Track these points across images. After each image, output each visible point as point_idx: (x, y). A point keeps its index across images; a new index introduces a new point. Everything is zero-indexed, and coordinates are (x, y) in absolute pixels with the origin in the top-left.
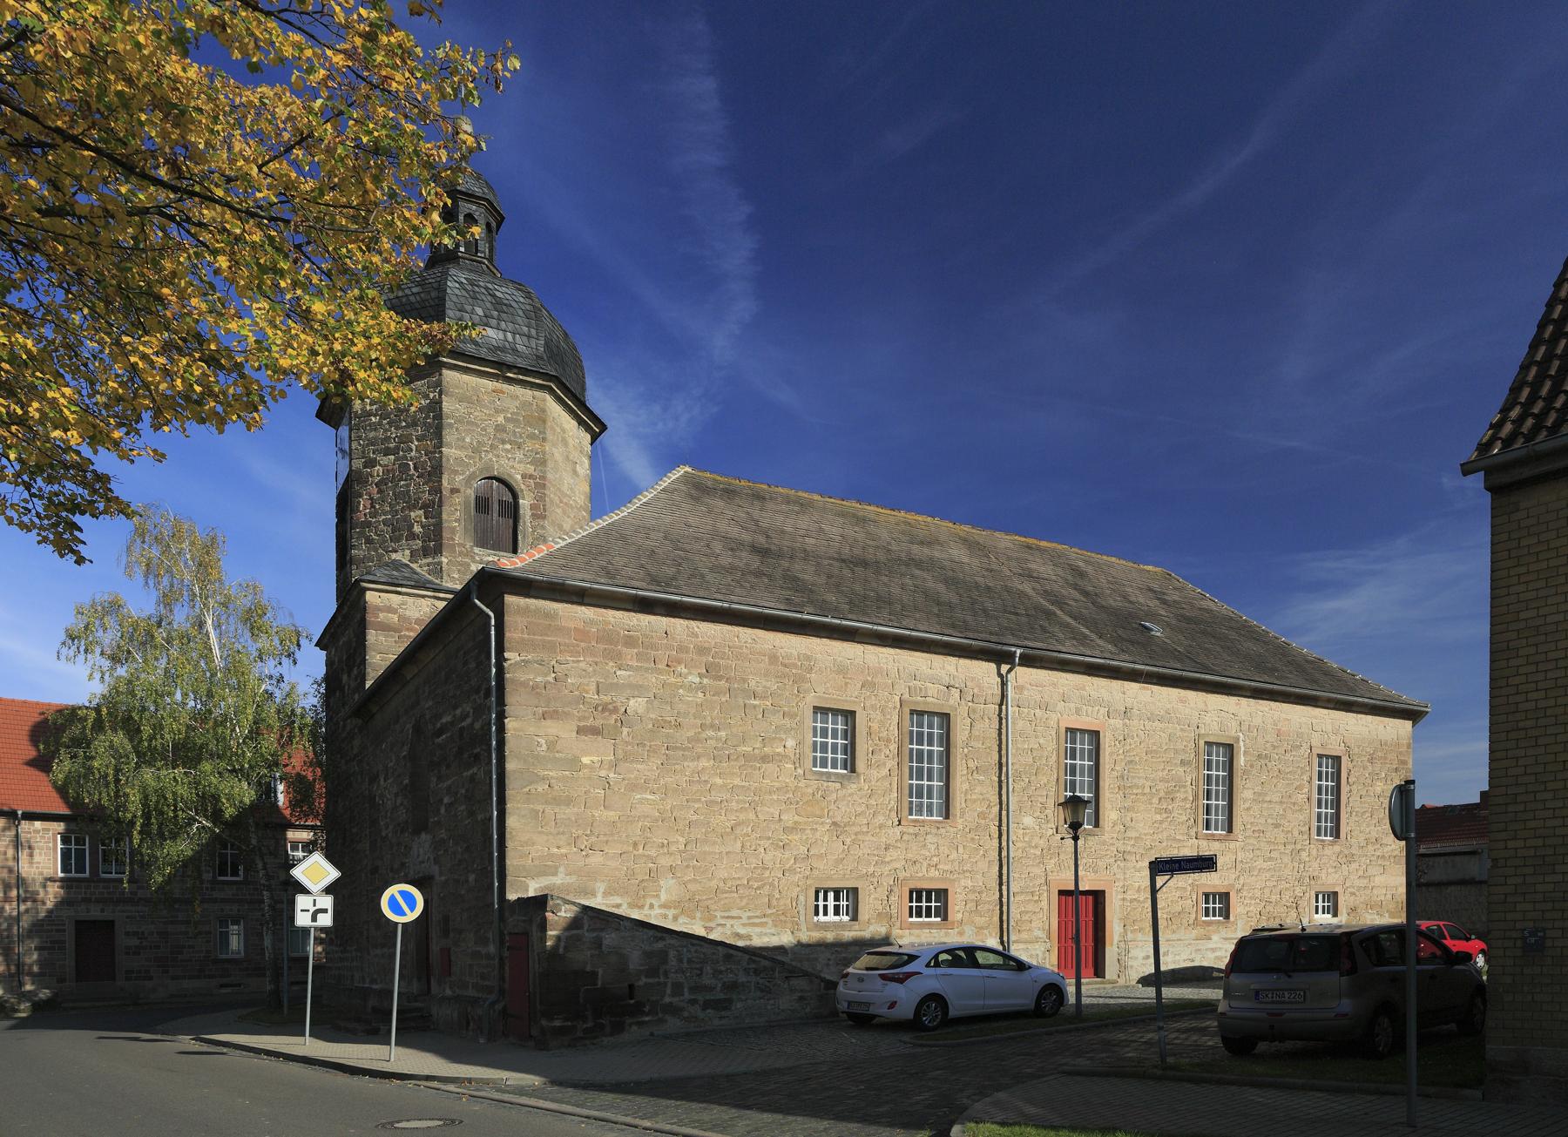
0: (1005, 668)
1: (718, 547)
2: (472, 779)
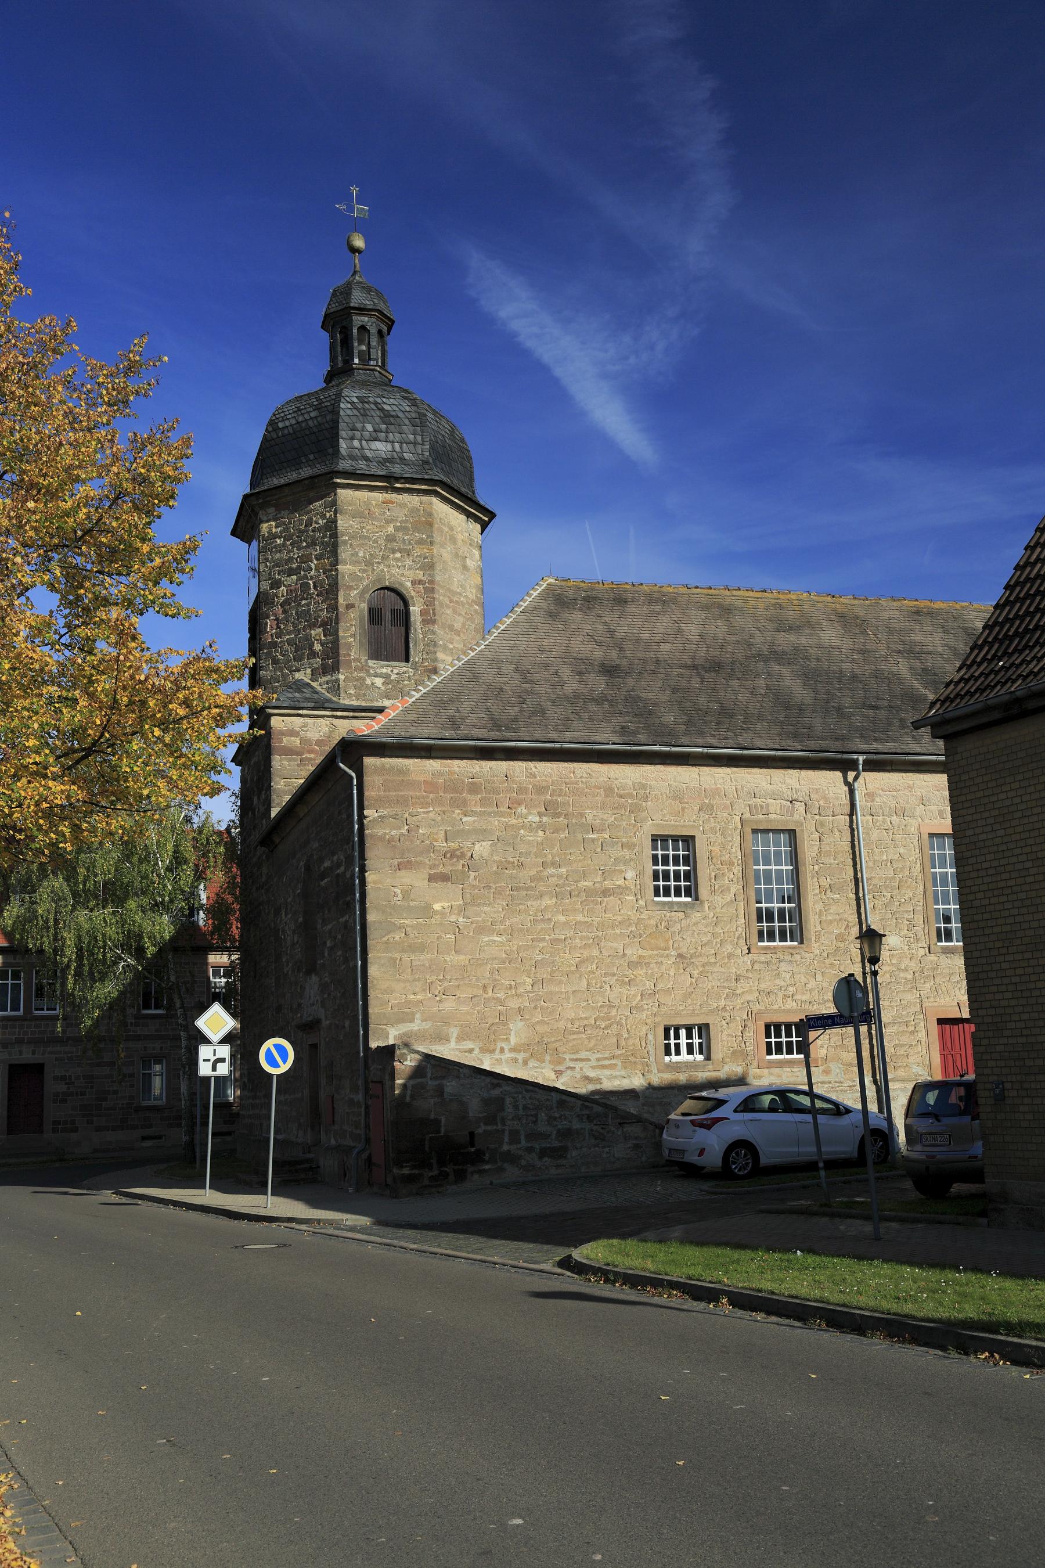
0: (851, 775)
1: (566, 671)
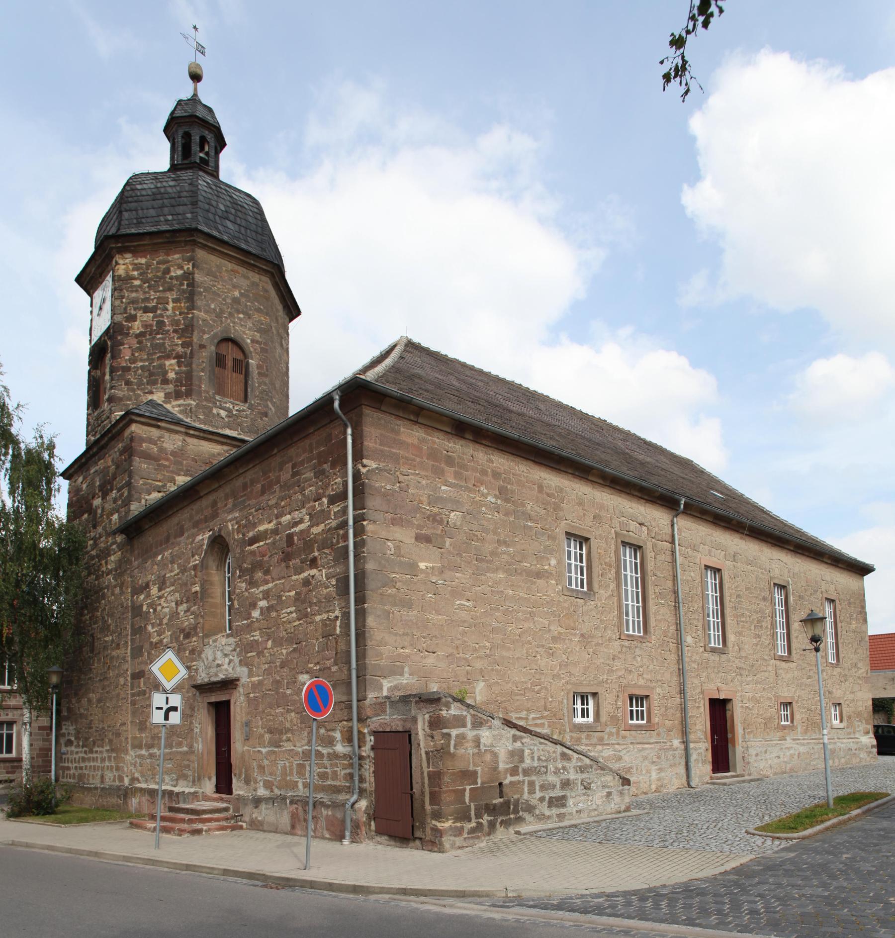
2: (307, 582)
